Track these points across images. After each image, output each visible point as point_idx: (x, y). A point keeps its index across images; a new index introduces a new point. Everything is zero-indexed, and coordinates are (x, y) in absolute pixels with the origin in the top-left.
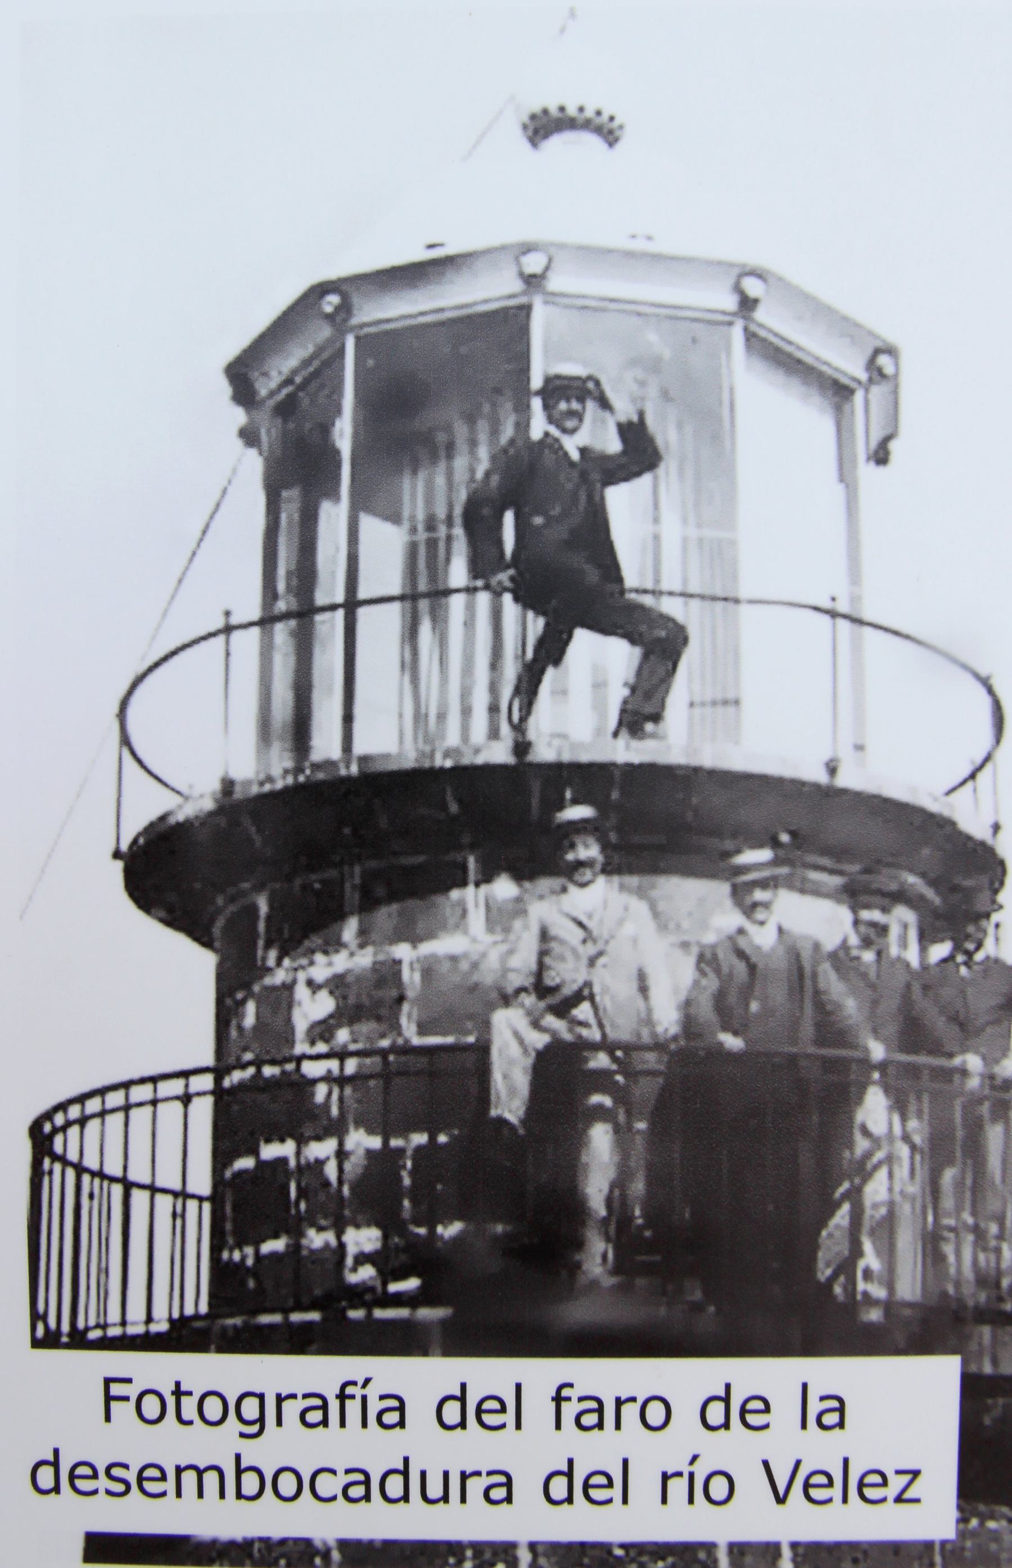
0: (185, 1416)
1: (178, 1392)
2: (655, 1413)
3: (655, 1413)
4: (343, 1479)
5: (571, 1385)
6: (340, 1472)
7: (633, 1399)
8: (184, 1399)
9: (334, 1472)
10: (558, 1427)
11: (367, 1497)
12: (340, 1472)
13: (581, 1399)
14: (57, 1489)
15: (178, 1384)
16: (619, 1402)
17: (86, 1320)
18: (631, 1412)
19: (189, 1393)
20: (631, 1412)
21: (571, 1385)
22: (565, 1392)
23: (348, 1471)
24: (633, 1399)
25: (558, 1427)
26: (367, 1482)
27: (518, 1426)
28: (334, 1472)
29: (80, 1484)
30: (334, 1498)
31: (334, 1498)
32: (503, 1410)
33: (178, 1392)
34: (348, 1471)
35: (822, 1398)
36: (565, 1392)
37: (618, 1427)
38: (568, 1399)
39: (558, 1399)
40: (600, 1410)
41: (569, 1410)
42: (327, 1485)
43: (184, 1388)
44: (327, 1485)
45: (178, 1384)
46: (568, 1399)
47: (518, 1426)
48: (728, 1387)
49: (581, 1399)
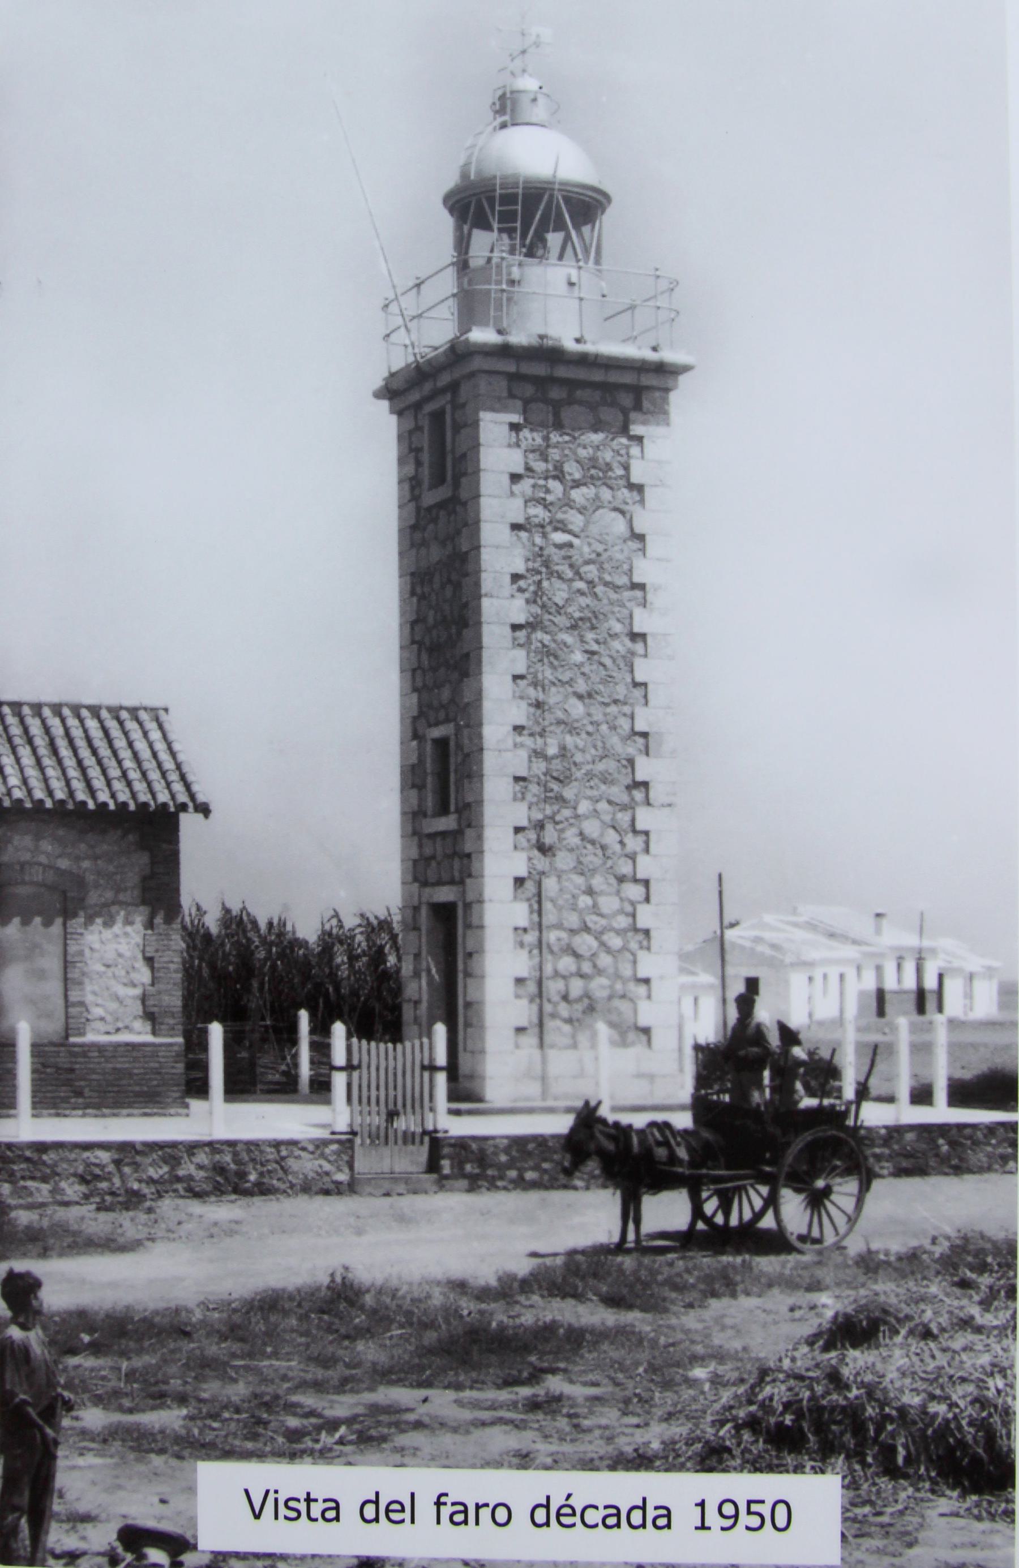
0: (313, 1515)
1: (309, 1500)
2: (501, 1515)
3: (501, 1515)
4: (603, 1512)
5: (446, 1495)
6: (601, 1508)
7: (487, 1505)
8: (312, 1504)
9: (596, 1508)
10: (438, 1522)
11: (618, 1525)
12: (601, 1508)
13: (453, 1504)
14: (377, 1520)
15: (308, 1494)
16: (478, 1507)
17: (404, 1048)
18: (485, 1513)
19: (316, 1500)
20: (485, 1513)
21: (446, 1495)
22: (443, 1499)
23: (606, 1507)
24: (487, 1505)
25: (438, 1522)
26: (618, 1515)
27: (413, 1521)
28: (596, 1508)
29: (393, 1516)
30: (596, 1525)
31: (596, 1525)
32: (403, 1510)
33: (309, 1500)
34: (606, 1507)
35: (656, 1508)
36: (443, 1499)
37: (477, 1523)
38: (445, 1504)
39: (438, 1504)
40: (465, 1512)
41: (446, 1511)
42: (592, 1516)
43: (312, 1496)
44: (592, 1516)
45: (308, 1494)
46: (445, 1504)
47: (413, 1521)
48: (548, 1498)
49: (453, 1504)
